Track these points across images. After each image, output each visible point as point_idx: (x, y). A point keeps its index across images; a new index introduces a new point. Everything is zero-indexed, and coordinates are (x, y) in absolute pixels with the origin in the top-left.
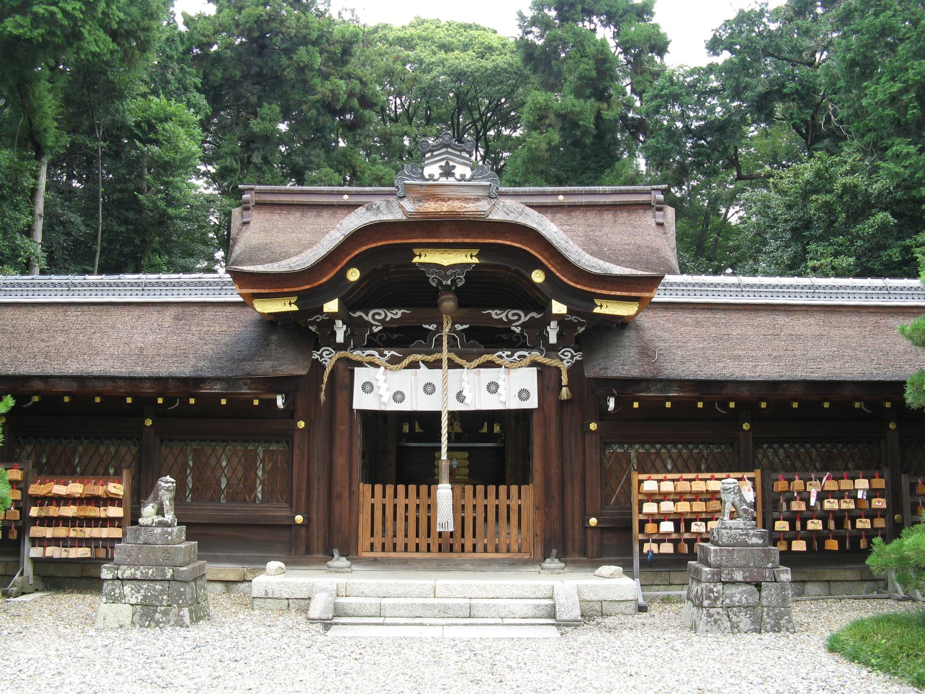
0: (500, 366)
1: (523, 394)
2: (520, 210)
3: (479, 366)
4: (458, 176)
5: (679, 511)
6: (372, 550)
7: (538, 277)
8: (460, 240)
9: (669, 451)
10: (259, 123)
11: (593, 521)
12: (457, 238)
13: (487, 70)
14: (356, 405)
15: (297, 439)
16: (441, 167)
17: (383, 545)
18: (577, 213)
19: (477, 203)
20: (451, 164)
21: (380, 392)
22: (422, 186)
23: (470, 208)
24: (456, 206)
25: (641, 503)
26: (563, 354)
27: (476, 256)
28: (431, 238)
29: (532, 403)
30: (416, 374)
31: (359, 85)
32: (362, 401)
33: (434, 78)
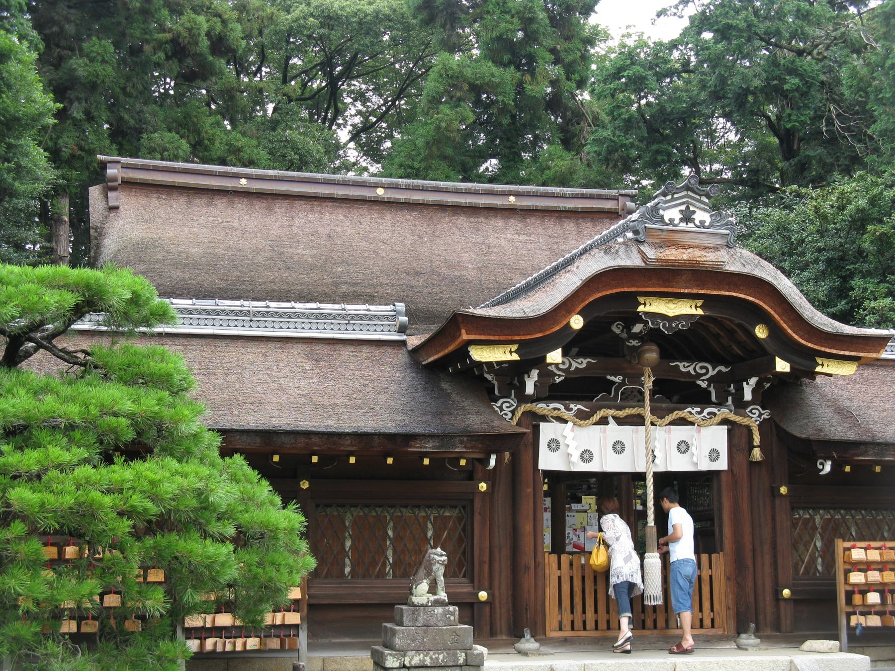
0: (692, 424)
1: (714, 455)
2: (756, 262)
3: (673, 423)
4: (697, 222)
5: (886, 581)
6: (561, 629)
7: (761, 332)
8: (695, 291)
9: (853, 517)
10: (86, 65)
11: (786, 592)
12: (692, 288)
13: (366, 15)
14: (543, 465)
15: (477, 505)
16: (681, 211)
17: (572, 622)
18: (533, 220)
19: (718, 253)
20: (692, 208)
21: (569, 451)
22: (662, 230)
23: (710, 257)
24: (696, 255)
25: (847, 572)
26: (751, 411)
27: (701, 307)
28: (666, 287)
29: (722, 464)
30: (605, 431)
31: (219, 24)
32: (548, 461)
33: (297, 20)
